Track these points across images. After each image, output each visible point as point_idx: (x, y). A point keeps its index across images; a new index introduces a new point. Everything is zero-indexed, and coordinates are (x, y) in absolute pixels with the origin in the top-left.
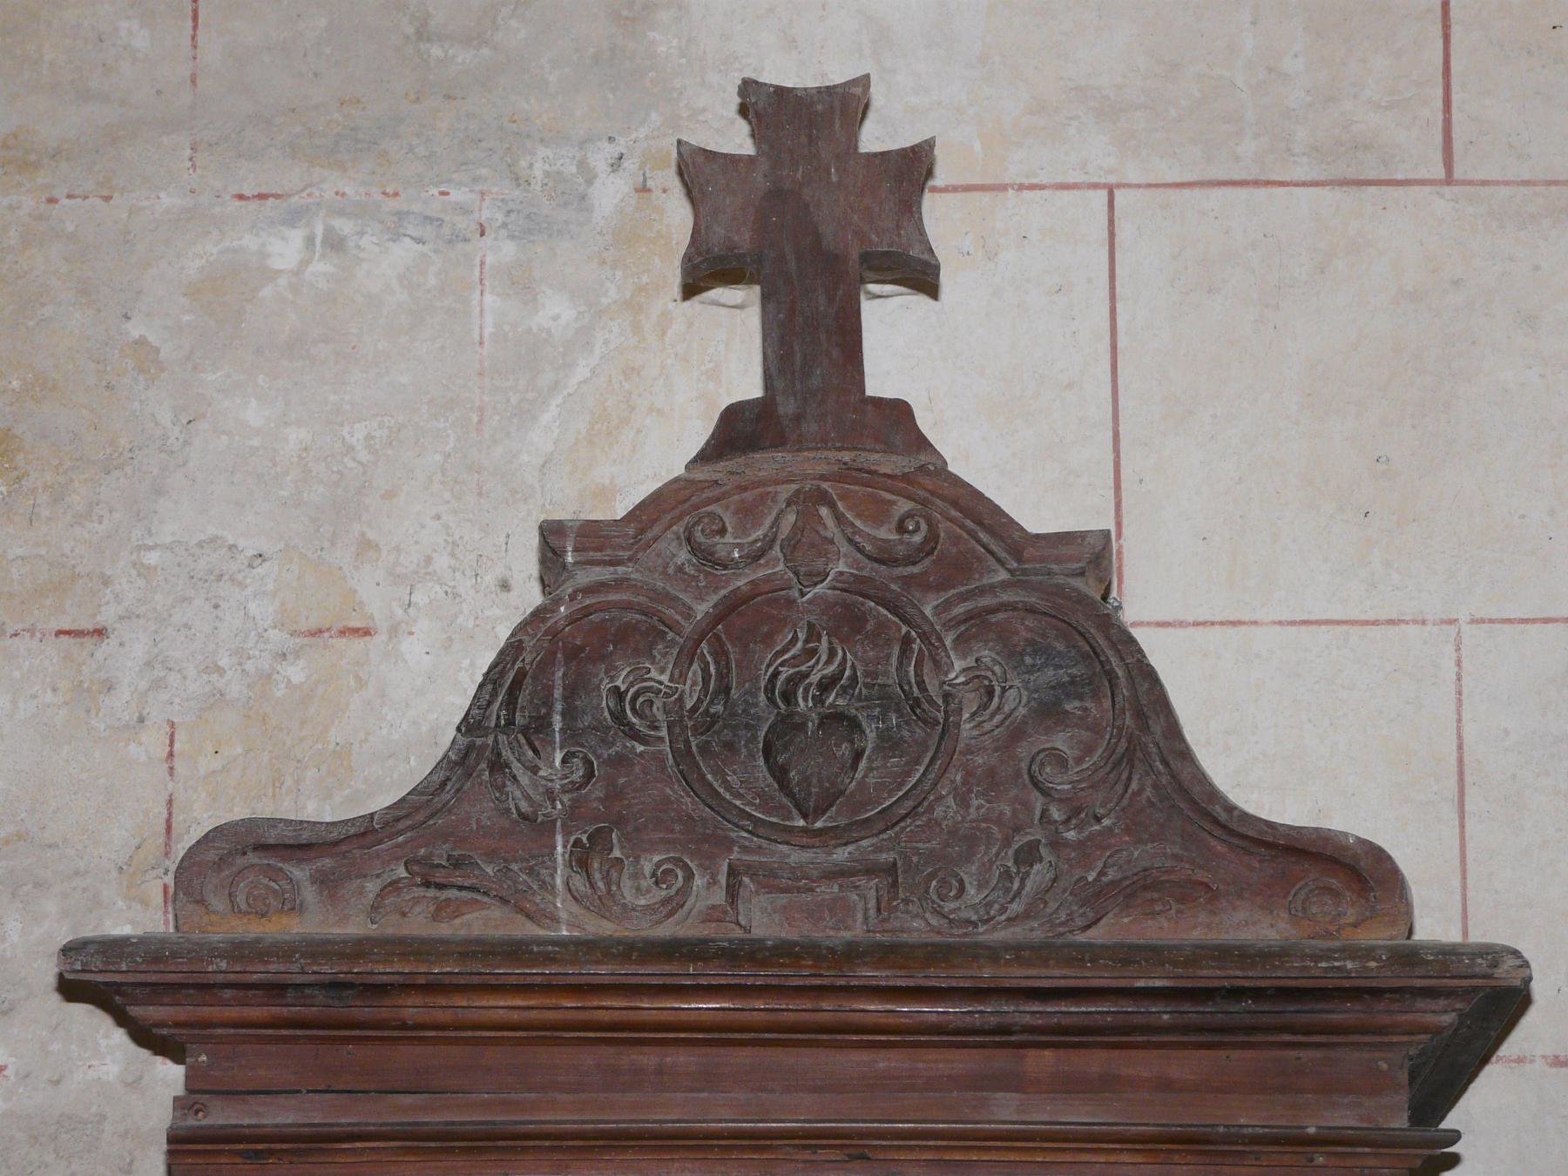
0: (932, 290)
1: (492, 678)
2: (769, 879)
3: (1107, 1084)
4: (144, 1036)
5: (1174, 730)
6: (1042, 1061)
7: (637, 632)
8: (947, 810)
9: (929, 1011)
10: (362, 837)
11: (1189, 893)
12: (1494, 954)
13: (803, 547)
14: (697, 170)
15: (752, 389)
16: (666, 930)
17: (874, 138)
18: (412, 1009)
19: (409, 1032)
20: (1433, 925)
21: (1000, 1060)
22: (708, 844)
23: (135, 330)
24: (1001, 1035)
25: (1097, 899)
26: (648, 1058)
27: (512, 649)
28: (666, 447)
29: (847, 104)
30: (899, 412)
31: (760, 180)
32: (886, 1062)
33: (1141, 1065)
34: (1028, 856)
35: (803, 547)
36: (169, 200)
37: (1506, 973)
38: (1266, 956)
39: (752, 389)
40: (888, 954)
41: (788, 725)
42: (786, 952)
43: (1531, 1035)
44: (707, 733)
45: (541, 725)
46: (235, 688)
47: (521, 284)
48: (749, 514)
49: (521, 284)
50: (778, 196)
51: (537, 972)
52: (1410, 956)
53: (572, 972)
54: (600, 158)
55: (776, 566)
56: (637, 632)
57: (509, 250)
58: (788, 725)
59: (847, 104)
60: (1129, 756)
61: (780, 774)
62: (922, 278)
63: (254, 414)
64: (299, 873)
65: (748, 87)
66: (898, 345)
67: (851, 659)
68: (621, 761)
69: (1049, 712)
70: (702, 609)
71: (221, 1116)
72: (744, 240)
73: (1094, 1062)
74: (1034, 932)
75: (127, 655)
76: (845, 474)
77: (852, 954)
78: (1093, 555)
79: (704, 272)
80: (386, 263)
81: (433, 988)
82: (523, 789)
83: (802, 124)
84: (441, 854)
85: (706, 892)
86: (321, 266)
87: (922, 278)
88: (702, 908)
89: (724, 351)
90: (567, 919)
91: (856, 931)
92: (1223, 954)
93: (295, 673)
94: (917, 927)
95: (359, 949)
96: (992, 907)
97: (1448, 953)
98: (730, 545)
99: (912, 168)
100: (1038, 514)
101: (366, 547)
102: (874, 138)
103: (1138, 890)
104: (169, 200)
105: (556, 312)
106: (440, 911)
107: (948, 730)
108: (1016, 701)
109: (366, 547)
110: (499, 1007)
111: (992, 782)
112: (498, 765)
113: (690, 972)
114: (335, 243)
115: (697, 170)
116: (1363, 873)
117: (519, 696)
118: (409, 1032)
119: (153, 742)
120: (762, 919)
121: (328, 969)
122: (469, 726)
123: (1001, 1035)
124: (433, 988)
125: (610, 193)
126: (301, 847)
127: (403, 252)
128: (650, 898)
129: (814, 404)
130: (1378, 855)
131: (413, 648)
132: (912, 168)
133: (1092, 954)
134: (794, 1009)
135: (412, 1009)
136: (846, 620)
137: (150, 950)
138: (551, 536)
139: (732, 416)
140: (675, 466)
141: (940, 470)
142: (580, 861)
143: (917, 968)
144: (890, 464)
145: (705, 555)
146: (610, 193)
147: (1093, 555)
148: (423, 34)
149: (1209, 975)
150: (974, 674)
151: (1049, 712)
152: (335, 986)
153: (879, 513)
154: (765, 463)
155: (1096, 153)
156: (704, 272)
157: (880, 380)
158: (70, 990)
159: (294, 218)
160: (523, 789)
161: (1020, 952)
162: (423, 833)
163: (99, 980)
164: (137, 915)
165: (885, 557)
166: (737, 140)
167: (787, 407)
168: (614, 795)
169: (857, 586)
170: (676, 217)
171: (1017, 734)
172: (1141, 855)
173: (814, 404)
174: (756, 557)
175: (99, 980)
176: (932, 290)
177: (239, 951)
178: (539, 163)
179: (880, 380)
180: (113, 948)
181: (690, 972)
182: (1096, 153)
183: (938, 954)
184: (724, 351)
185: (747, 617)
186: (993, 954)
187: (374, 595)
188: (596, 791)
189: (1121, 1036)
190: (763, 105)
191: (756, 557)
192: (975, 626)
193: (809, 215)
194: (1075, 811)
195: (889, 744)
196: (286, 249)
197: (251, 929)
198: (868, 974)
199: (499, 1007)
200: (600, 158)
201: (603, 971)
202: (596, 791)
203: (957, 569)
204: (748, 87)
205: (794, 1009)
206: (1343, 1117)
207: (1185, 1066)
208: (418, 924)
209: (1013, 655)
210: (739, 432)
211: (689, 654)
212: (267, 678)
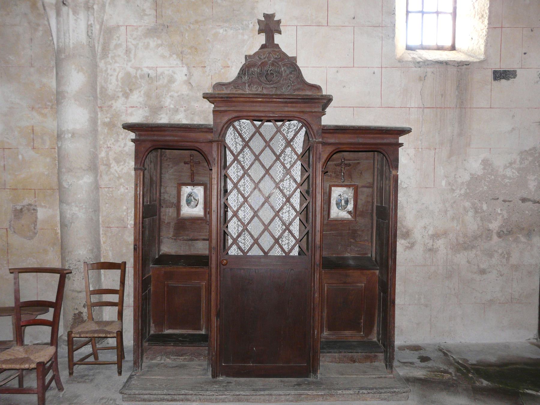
0: (281, 34)
1: (241, 69)
2: (266, 88)
3: (296, 107)
4: (210, 102)
5: (302, 75)
6: (290, 105)
7: (254, 65)
8: (281, 82)
9: (280, 100)
10: (230, 84)
11: (303, 90)
12: (330, 96)
13: (269, 58)
14: (259, 22)
15: (264, 43)
16: (256, 93)
17: (276, 19)
18: (234, 99)
19: (234, 102)
20: (324, 93)
21: (286, 105)
22: (260, 85)
23: (208, 38)
24: (286, 102)
25: (295, 90)
26: (255, 104)
27: (243, 67)
28: (256, 48)
29: (273, 15)
30: (278, 45)
31: (265, 23)
32: (276, 105)
33: (299, 105)
34: (289, 86)
35: (269, 58)
36: (211, 26)
37: (331, 97)
38: (310, 95)
39: (264, 43)
40: (276, 95)
41: (267, 74)
42: (267, 95)
43: (332, 104)
44: (260, 74)
45: (245, 74)
46: (217, 72)
47: (243, 34)
48: (264, 54)
49: (243, 34)
50: (267, 24)
51: (245, 96)
52: (322, 96)
53: (248, 96)
54: (250, 23)
55: (266, 59)
56: (254, 65)
57: (242, 31)
58: (267, 74)
59: (273, 15)
60: (298, 77)
61: (267, 78)
62: (280, 32)
63: (219, 47)
64: (224, 87)
65: (264, 14)
66: (278, 39)
67: (273, 68)
68: (252, 77)
69: (291, 73)
70: (260, 63)
71: (217, 109)
72: (264, 28)
73: (294, 105)
74: (289, 93)
75: (207, 69)
76: (273, 51)
77: (273, 95)
78: (295, 58)
79: (260, 31)
80: (230, 32)
81: (236, 97)
82: (243, 80)
83: (269, 17)
84: (236, 85)
85: (260, 89)
86: (225, 33)
87: (280, 32)
88: (259, 91)
89: (262, 39)
90: (248, 92)
91: (273, 93)
92: (307, 95)
93: (223, 71)
94: (279, 93)
95: (229, 94)
96: (285, 91)
97: (325, 95)
98: (262, 57)
99: (279, 22)
100: (290, 55)
101: (229, 59)
102: (276, 19)
103: (298, 89)
104: (211, 26)
105: (246, 37)
106: (236, 91)
107: (282, 75)
108: (288, 72)
109: (229, 59)
110: (242, 99)
111: (286, 80)
112: (241, 77)
113: (259, 96)
114: (226, 30)
115: (259, 22)
116: (318, 88)
117: (243, 71)
118: (234, 102)
119: (210, 77)
120: (265, 92)
121: (226, 96)
122: (239, 74)
123: (286, 102)
124: (236, 97)
125: (251, 26)
126: (62, 249)
127: (232, 31)
128: (255, 90)
129: (270, 45)
130: (320, 87)
131: (233, 68)
132: (279, 22)
133: (294, 95)
134: (268, 100)
135: (234, 99)
136: (273, 64)
137: (211, 94)
138: (246, 56)
139: (262, 45)
140: (257, 50)
141: (281, 51)
142: (249, 86)
143: (279, 96)
144: (276, 50)
145: (260, 58)
146: (251, 26)
147: (295, 58)
148: (234, 10)
149: (305, 97)
150: (284, 70)
151: (291, 73)
152: (227, 97)
153: (275, 54)
154: (266, 50)
155: (295, 22)
156: (260, 31)
157: (276, 42)
158: (204, 97)
159: (222, 28)
160: (243, 80)
161: (288, 95)
162: (235, 83)
163: (207, 97)
164: (210, 91)
165: (276, 59)
166: (263, 19)
167: (267, 44)
168: (252, 80)
169: (273, 61)
170: (257, 27)
171: (288, 75)
172: (298, 86)
173: (270, 45)
174: (264, 58)
175: (207, 97)
176: (281, 34)
177: (218, 94)
178: (244, 23)
179: (276, 42)
180: (207, 94)
181: (259, 96)
182: (295, 22)
183: (280, 95)
184: (262, 39)
185: (263, 64)
186: (285, 95)
187: (230, 64)
188: (250, 80)
189: (296, 103)
190: (266, 16)
191: (264, 58)
192: (284, 65)
193: (269, 26)
194: (293, 82)
195: (276, 76)
196: (221, 31)
197: (219, 92)
198: (274, 97)
199: (242, 99)
200: (250, 23)
201: (251, 96)
202: (250, 80)
203: (283, 60)
204: (264, 14)
205: (268, 100)
206: (316, 110)
207: (302, 105)
208: (234, 92)
209: (288, 68)
210: (263, 47)
211: (258, 67)
212: (220, 71)
